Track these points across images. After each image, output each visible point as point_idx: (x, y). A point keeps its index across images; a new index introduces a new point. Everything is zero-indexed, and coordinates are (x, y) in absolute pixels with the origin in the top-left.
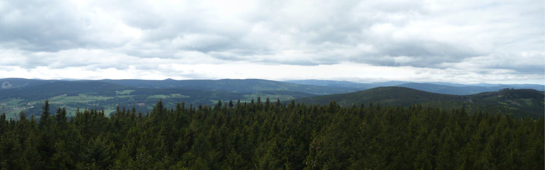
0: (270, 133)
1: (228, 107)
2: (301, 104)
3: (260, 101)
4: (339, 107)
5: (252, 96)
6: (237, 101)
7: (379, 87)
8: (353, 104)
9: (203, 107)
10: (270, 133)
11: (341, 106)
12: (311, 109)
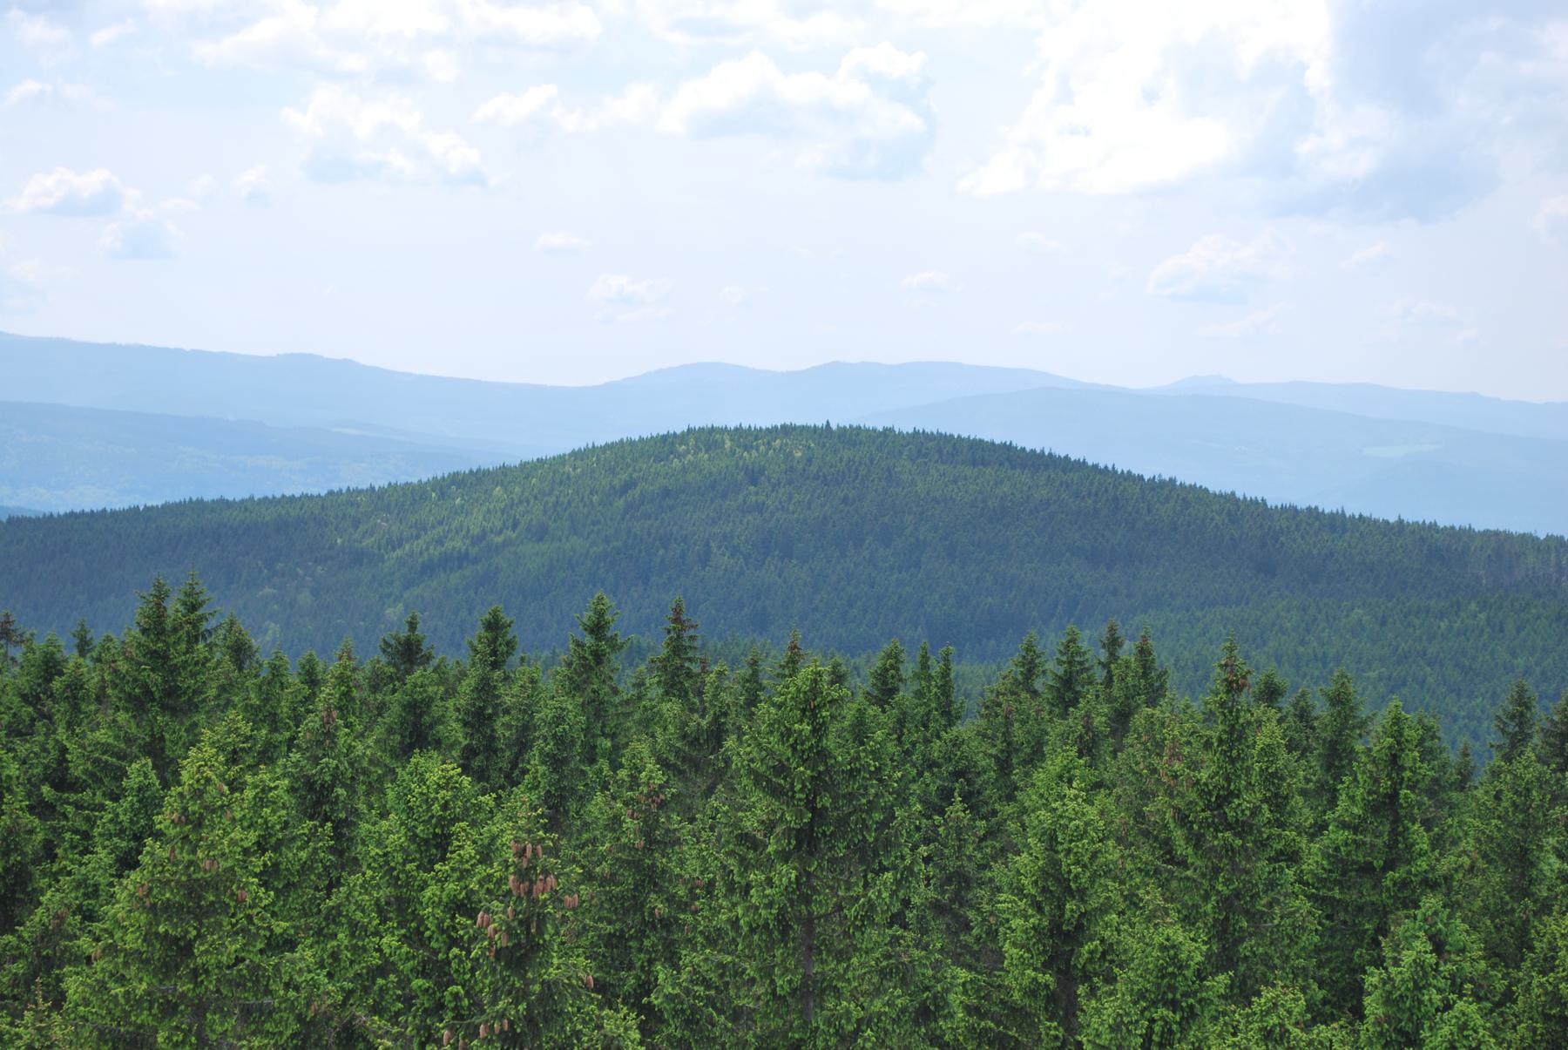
4: (240, 652)
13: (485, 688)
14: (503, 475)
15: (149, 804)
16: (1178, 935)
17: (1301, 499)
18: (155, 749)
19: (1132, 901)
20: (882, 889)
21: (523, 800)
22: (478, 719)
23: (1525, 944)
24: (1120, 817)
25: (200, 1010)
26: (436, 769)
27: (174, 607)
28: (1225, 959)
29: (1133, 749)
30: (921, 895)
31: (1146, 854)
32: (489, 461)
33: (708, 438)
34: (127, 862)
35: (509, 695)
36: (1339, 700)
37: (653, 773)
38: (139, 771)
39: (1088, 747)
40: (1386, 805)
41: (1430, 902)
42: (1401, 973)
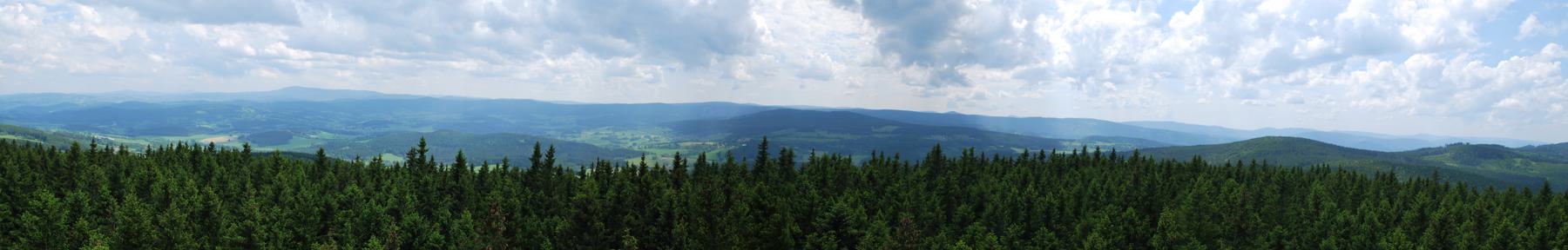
1: (1038, 161)
2: (1147, 158)
4: (1206, 164)
5: (1074, 144)
6: (1051, 151)
9: (1001, 158)
11: (1209, 163)
12: (1161, 167)
13: (1238, 170)
14: (1241, 142)
15: (1193, 184)
16: (1333, 203)
17: (1348, 146)
18: (1194, 177)
19: (1327, 199)
20: (1292, 198)
21: (1244, 185)
22: (1237, 174)
23: (1378, 204)
24: (1325, 188)
25: (1200, 211)
26: (1232, 180)
27: (1197, 158)
28: (1339, 207)
29: (1327, 179)
30: (1298, 199)
31: (1328, 193)
32: (1239, 140)
33: (1269, 137)
34: (1190, 192)
35: (1242, 171)
36: (1354, 173)
37: (1261, 181)
38: (1192, 180)
39: (1320, 179)
40: (1361, 187)
41: (1367, 199)
42: (1362, 207)
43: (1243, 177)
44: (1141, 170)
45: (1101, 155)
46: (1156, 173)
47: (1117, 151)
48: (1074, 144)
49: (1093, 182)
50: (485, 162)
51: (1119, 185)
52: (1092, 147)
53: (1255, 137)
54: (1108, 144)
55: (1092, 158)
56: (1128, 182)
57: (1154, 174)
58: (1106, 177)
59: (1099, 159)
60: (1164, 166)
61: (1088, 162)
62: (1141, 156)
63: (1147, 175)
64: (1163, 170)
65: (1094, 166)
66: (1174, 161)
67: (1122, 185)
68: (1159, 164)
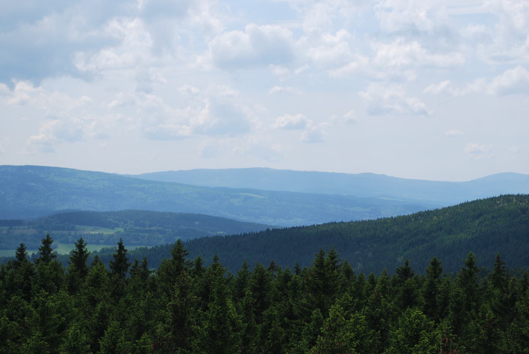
0: (204, 231)
2: (207, 264)
3: (50, 250)
4: (349, 273)
5: (18, 231)
7: (497, 195)
8: (400, 259)
10: (204, 231)
11: (357, 269)
12: (242, 284)
13: (432, 285)
14: (436, 212)
15: (319, 324)
21: (445, 324)
22: (430, 295)
26: (416, 312)
32: (432, 208)
33: (507, 198)
38: (316, 313)
43: (445, 303)
44: (192, 296)
45: (88, 263)
46: (230, 303)
47: (129, 248)
48: (18, 231)
49: (70, 332)
50: (81, 241)
51: (139, 337)
52: (66, 242)
53: (471, 199)
54: (107, 232)
55: (67, 268)
56: (160, 328)
57: (223, 304)
58: (103, 317)
59: (84, 273)
60: (250, 281)
61: (58, 281)
62: (190, 259)
63: (206, 308)
64: (248, 291)
65: (73, 289)
66: (272, 267)
67: (145, 336)
68: (236, 277)
